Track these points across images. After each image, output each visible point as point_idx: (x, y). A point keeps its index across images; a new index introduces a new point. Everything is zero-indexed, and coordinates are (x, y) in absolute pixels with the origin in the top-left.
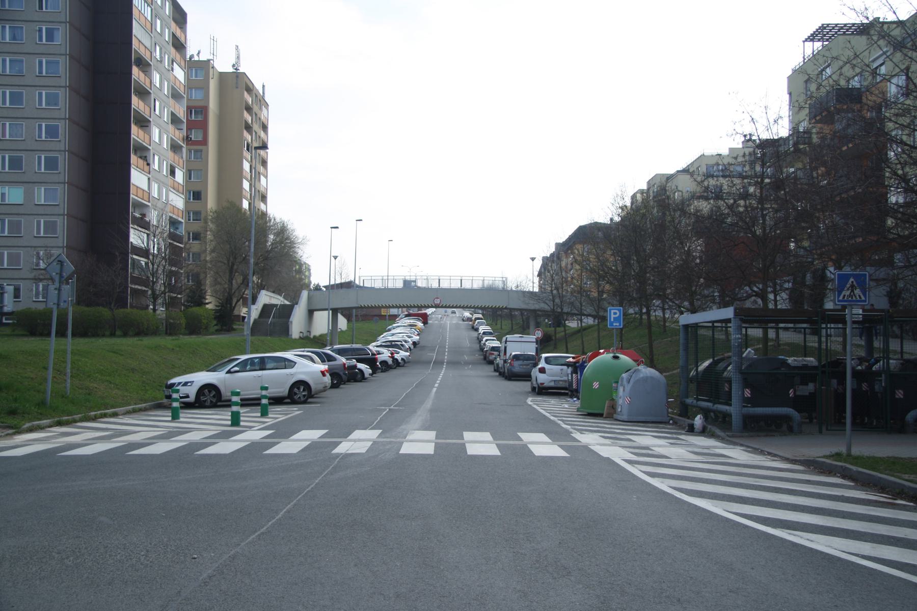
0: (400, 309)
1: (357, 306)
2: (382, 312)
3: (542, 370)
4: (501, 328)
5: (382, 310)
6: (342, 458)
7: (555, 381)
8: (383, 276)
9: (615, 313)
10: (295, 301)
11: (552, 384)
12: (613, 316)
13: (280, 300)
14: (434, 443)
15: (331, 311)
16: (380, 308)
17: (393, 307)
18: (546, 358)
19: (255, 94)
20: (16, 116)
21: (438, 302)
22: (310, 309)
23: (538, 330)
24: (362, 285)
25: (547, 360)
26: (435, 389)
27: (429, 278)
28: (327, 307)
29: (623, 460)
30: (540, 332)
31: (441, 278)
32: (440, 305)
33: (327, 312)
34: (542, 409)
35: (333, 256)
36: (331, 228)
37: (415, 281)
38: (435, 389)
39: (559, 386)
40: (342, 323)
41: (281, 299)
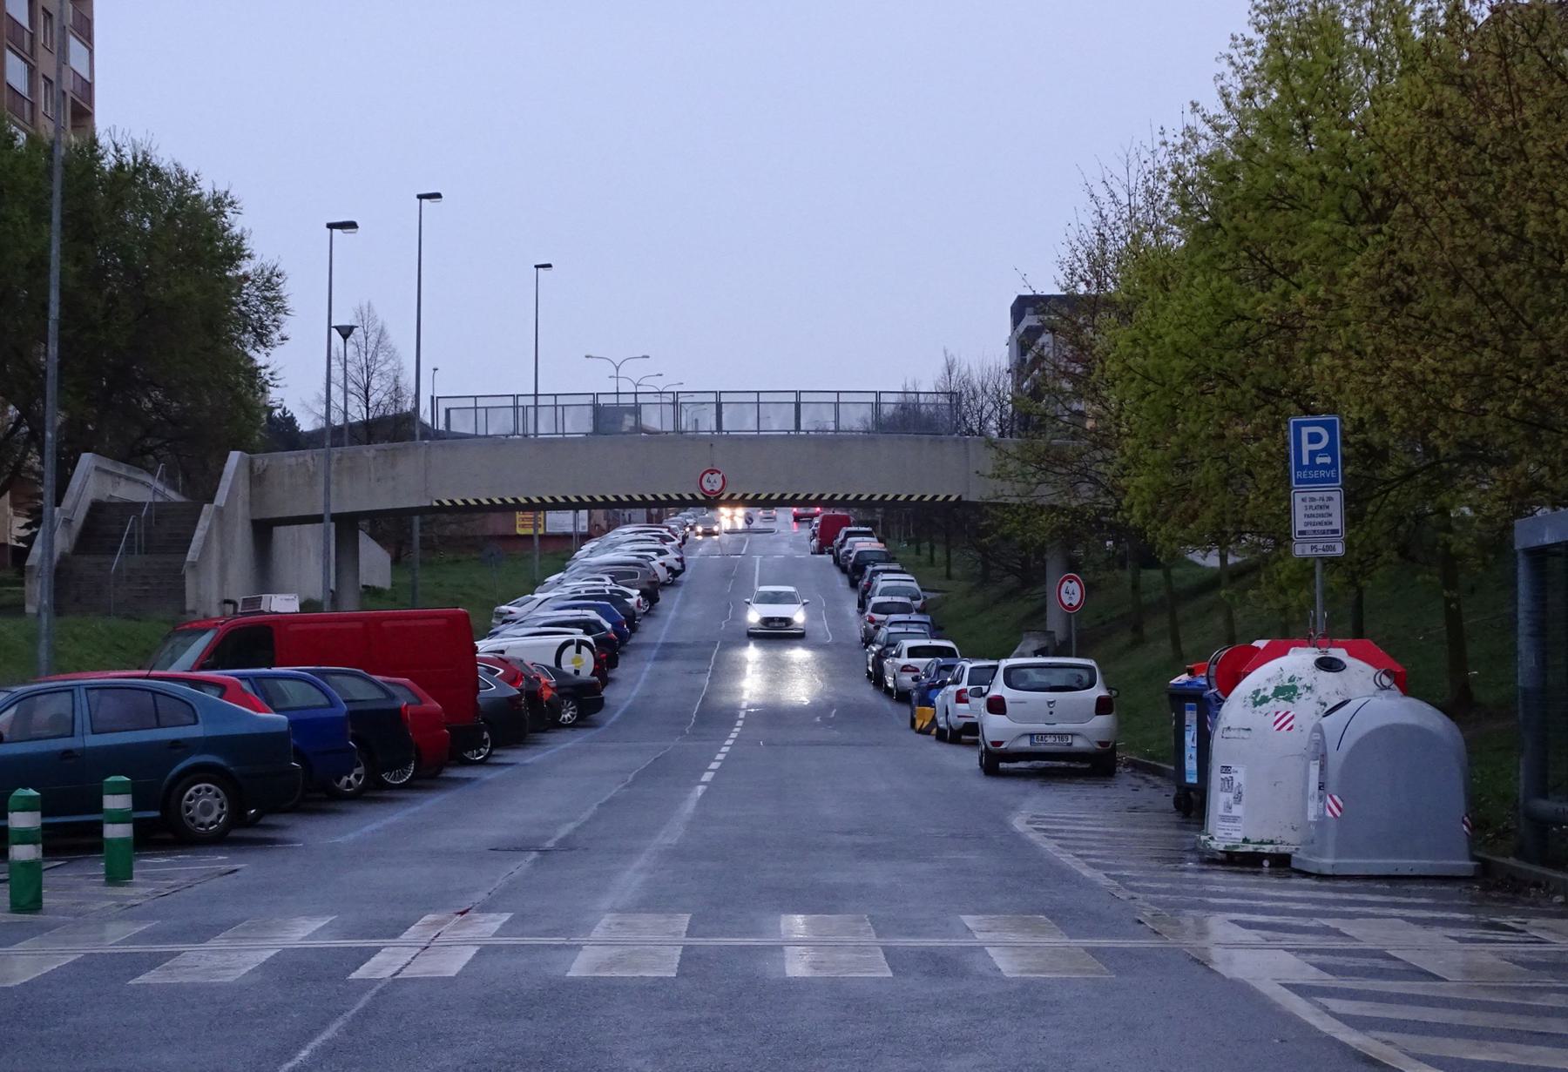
0: (584, 513)
3: (997, 706)
5: (519, 515)
6: (381, 992)
7: (1032, 735)
8: (516, 397)
9: (1315, 438)
10: (201, 486)
11: (1025, 744)
12: (1307, 447)
13: (149, 486)
15: (333, 525)
16: (508, 509)
17: (556, 506)
18: (1008, 670)
19: (44, 9)
21: (717, 488)
23: (1071, 580)
24: (442, 426)
25: (1011, 678)
26: (700, 789)
27: (804, 398)
28: (320, 511)
29: (1285, 985)
30: (1075, 586)
31: (724, 398)
33: (318, 527)
34: (1095, 866)
35: (336, 327)
36: (331, 226)
37: (636, 410)
38: (700, 789)
39: (1043, 748)
40: (375, 564)
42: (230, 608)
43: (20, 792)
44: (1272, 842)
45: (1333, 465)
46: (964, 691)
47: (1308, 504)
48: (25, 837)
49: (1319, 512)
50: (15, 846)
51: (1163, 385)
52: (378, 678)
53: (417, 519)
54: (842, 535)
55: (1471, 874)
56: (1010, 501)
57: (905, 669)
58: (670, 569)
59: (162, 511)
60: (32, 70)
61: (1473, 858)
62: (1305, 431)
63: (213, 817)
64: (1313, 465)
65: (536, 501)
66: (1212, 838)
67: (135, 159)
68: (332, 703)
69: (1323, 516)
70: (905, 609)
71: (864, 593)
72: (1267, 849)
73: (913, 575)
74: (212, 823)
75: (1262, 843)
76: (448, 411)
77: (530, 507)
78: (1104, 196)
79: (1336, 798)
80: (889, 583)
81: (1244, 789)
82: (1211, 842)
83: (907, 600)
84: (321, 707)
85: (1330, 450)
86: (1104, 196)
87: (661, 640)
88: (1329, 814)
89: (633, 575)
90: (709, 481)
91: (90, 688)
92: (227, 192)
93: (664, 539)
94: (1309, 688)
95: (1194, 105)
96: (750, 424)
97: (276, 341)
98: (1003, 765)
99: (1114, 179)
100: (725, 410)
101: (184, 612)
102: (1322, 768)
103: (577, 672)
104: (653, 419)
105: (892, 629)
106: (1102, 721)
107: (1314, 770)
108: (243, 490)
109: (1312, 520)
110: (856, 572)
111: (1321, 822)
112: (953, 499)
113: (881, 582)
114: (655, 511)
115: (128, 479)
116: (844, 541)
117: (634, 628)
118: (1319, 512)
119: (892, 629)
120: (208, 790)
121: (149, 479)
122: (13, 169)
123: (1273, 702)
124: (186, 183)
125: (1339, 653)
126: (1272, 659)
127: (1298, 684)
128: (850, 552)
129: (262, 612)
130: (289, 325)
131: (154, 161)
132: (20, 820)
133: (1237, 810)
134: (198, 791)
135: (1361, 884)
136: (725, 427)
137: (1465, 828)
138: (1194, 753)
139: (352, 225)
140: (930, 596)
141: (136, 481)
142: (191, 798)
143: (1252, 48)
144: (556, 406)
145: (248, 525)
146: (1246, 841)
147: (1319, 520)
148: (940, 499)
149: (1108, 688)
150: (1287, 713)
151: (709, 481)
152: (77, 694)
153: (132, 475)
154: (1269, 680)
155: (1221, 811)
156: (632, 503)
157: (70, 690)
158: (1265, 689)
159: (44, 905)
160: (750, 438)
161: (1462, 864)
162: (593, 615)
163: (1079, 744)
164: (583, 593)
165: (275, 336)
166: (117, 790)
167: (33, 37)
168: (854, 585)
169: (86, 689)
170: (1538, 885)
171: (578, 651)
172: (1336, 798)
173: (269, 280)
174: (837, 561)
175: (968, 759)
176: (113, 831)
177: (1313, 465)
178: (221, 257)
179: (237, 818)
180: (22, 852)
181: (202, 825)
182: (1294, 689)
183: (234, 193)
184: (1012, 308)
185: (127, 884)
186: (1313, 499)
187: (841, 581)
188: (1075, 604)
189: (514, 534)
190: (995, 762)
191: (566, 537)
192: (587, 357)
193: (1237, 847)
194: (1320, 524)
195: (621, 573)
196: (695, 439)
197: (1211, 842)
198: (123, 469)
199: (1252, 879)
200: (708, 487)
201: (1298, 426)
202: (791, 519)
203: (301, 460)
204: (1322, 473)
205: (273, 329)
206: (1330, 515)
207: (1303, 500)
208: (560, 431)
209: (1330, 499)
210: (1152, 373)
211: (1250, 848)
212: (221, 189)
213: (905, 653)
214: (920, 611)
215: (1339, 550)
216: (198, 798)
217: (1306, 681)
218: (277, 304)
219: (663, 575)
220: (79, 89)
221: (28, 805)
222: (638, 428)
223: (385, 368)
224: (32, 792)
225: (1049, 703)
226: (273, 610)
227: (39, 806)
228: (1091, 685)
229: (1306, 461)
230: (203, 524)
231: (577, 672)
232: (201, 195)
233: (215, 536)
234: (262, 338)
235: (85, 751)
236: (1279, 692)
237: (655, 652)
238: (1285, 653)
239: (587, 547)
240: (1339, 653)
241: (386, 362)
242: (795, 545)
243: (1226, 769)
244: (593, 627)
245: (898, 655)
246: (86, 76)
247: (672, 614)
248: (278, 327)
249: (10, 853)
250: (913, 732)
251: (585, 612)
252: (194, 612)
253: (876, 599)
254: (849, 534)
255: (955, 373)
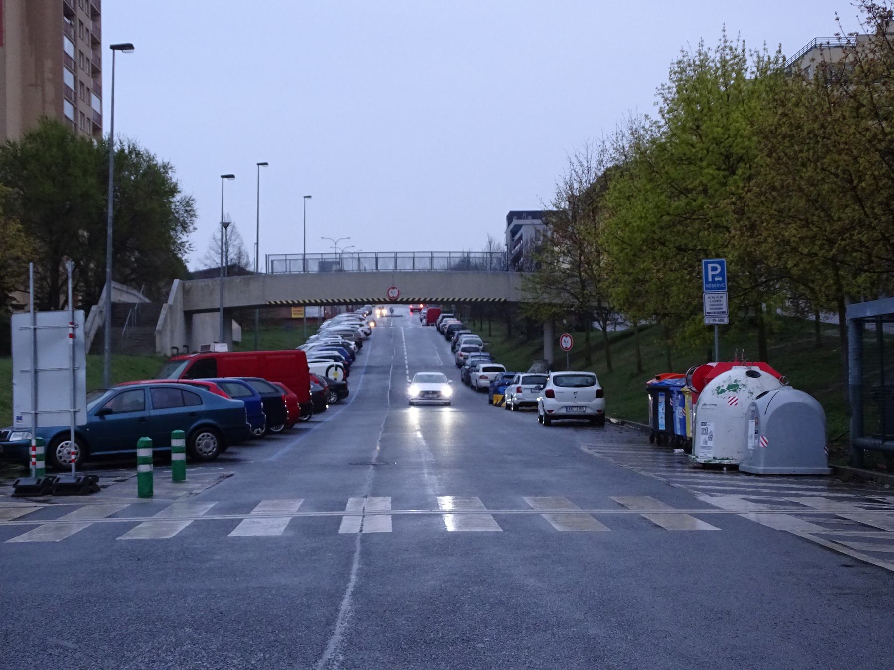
1: (263, 303)
2: (293, 313)
3: (550, 394)
4: (490, 336)
5: (293, 309)
7: (566, 407)
9: (714, 269)
10: (159, 298)
11: (563, 411)
12: (710, 273)
14: (391, 516)
16: (289, 305)
17: (311, 304)
18: (555, 378)
20: (398, 264)
21: (396, 295)
22: (186, 309)
25: (556, 381)
31: (399, 255)
32: (399, 300)
39: (571, 413)
41: (140, 296)
42: (175, 351)
43: (143, 439)
44: (727, 459)
45: (723, 281)
46: (520, 387)
47: (711, 299)
48: (145, 461)
49: (716, 303)
50: (141, 465)
51: (631, 245)
52: (271, 383)
53: (257, 310)
54: (440, 317)
55: (829, 474)
56: (530, 301)
57: (481, 377)
58: (365, 333)
59: (143, 306)
60: (75, 109)
61: (830, 467)
62: (710, 266)
63: (210, 449)
64: (713, 282)
65: (296, 302)
66: (697, 457)
67: (129, 147)
68: (253, 394)
69: (718, 305)
70: (476, 350)
71: (455, 343)
72: (726, 462)
73: (477, 335)
74: (210, 452)
75: (723, 459)
76: (272, 261)
77: (299, 305)
78: (574, 160)
79: (765, 438)
80: (467, 338)
81: (714, 434)
82: (697, 459)
83: (477, 346)
84: (249, 396)
85: (721, 274)
86: (574, 160)
87: (365, 365)
88: (761, 445)
89: (351, 335)
90: (392, 292)
91: (151, 388)
92: (169, 163)
93: (361, 319)
94: (744, 385)
95: (646, 116)
96: (391, 267)
97: (191, 230)
98: (553, 421)
99: (580, 155)
100: (399, 261)
101: (155, 352)
102: (757, 424)
103: (336, 379)
104: (350, 266)
105: (473, 359)
106: (599, 401)
107: (752, 425)
108: (180, 296)
109: (713, 307)
110: (449, 334)
111: (756, 450)
112: (502, 300)
113: (464, 338)
114: (350, 307)
115: (127, 292)
116: (442, 320)
117: (354, 359)
118: (716, 303)
119: (473, 359)
120: (208, 436)
121: (135, 292)
122: (74, 152)
123: (727, 392)
124: (150, 159)
125: (756, 369)
126: (722, 373)
127: (739, 383)
128: (445, 325)
129: (210, 352)
130: (197, 223)
131: (138, 149)
132: (143, 453)
133: (710, 444)
134: (203, 436)
135: (785, 479)
136: (379, 268)
137: (826, 452)
138: (663, 416)
139: (232, 176)
140: (486, 344)
141: (130, 294)
142: (200, 440)
143: (670, 90)
144: (286, 260)
145: (182, 315)
146: (715, 458)
147: (717, 307)
148: (479, 300)
149: (601, 386)
150: (734, 397)
151: (392, 292)
152: (146, 391)
153: (129, 291)
154: (724, 382)
155: (702, 444)
156: (340, 303)
157: (142, 389)
158: (723, 386)
159: (154, 494)
160: (410, 273)
161: (825, 469)
162: (336, 353)
163: (589, 411)
164: (329, 344)
165: (191, 228)
166: (179, 437)
167: (75, 94)
168: (448, 339)
169: (151, 388)
170: (872, 479)
171: (336, 370)
172: (765, 438)
173: (188, 202)
174: (438, 329)
175: (532, 419)
176: (176, 457)
177: (713, 282)
178: (166, 192)
179: (222, 447)
180: (144, 468)
181: (205, 452)
182: (737, 386)
183: (172, 163)
184: (507, 217)
185: (183, 483)
186: (713, 298)
187: (441, 339)
188: (568, 347)
189: (289, 317)
190: (549, 420)
191: (314, 319)
192: (322, 238)
193: (711, 461)
194: (717, 309)
195: (345, 334)
196: (386, 274)
197: (697, 459)
198: (124, 288)
199: (718, 476)
200: (391, 295)
201: (706, 263)
202: (409, 311)
203: (206, 284)
204: (718, 285)
205: (190, 224)
206: (722, 305)
207: (709, 298)
208: (288, 270)
209: (722, 297)
210: (626, 239)
211: (717, 461)
212: (166, 161)
213: (481, 370)
214: (483, 351)
215: (726, 321)
216: (203, 440)
217: (743, 382)
218: (192, 213)
219: (363, 335)
220: (96, 118)
221: (146, 446)
222: (341, 271)
223: (236, 243)
224: (148, 439)
225: (575, 393)
226: (216, 351)
227: (185, 450)
228: (593, 384)
229: (710, 279)
230: (163, 312)
231: (336, 379)
232: (157, 164)
233: (168, 318)
234: (185, 228)
235: (150, 417)
236: (730, 387)
237: (363, 370)
238: (730, 369)
239: (326, 323)
240: (756, 369)
241: (236, 240)
242: (414, 321)
243: (705, 424)
244: (338, 359)
245: (478, 371)
246: (99, 112)
247: (368, 353)
248: (192, 224)
249: (138, 468)
250: (491, 407)
251: (334, 352)
252: (160, 353)
253: (463, 346)
254: (443, 317)
255: (492, 244)
